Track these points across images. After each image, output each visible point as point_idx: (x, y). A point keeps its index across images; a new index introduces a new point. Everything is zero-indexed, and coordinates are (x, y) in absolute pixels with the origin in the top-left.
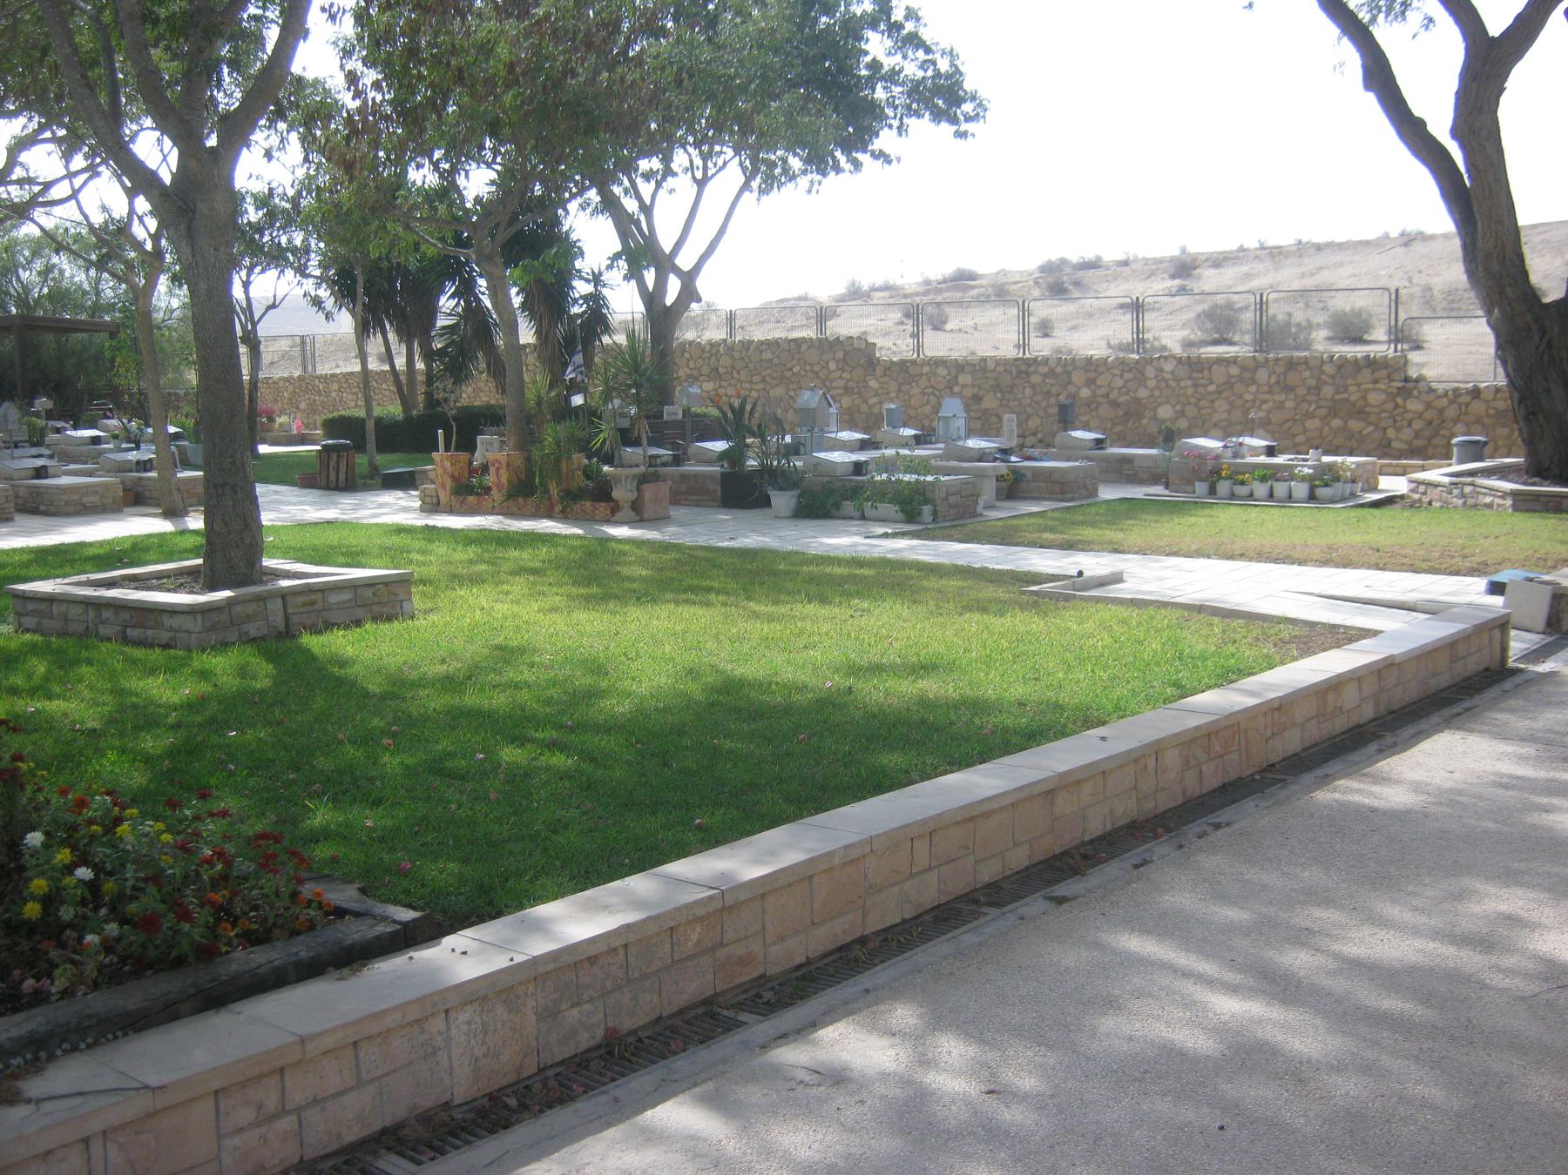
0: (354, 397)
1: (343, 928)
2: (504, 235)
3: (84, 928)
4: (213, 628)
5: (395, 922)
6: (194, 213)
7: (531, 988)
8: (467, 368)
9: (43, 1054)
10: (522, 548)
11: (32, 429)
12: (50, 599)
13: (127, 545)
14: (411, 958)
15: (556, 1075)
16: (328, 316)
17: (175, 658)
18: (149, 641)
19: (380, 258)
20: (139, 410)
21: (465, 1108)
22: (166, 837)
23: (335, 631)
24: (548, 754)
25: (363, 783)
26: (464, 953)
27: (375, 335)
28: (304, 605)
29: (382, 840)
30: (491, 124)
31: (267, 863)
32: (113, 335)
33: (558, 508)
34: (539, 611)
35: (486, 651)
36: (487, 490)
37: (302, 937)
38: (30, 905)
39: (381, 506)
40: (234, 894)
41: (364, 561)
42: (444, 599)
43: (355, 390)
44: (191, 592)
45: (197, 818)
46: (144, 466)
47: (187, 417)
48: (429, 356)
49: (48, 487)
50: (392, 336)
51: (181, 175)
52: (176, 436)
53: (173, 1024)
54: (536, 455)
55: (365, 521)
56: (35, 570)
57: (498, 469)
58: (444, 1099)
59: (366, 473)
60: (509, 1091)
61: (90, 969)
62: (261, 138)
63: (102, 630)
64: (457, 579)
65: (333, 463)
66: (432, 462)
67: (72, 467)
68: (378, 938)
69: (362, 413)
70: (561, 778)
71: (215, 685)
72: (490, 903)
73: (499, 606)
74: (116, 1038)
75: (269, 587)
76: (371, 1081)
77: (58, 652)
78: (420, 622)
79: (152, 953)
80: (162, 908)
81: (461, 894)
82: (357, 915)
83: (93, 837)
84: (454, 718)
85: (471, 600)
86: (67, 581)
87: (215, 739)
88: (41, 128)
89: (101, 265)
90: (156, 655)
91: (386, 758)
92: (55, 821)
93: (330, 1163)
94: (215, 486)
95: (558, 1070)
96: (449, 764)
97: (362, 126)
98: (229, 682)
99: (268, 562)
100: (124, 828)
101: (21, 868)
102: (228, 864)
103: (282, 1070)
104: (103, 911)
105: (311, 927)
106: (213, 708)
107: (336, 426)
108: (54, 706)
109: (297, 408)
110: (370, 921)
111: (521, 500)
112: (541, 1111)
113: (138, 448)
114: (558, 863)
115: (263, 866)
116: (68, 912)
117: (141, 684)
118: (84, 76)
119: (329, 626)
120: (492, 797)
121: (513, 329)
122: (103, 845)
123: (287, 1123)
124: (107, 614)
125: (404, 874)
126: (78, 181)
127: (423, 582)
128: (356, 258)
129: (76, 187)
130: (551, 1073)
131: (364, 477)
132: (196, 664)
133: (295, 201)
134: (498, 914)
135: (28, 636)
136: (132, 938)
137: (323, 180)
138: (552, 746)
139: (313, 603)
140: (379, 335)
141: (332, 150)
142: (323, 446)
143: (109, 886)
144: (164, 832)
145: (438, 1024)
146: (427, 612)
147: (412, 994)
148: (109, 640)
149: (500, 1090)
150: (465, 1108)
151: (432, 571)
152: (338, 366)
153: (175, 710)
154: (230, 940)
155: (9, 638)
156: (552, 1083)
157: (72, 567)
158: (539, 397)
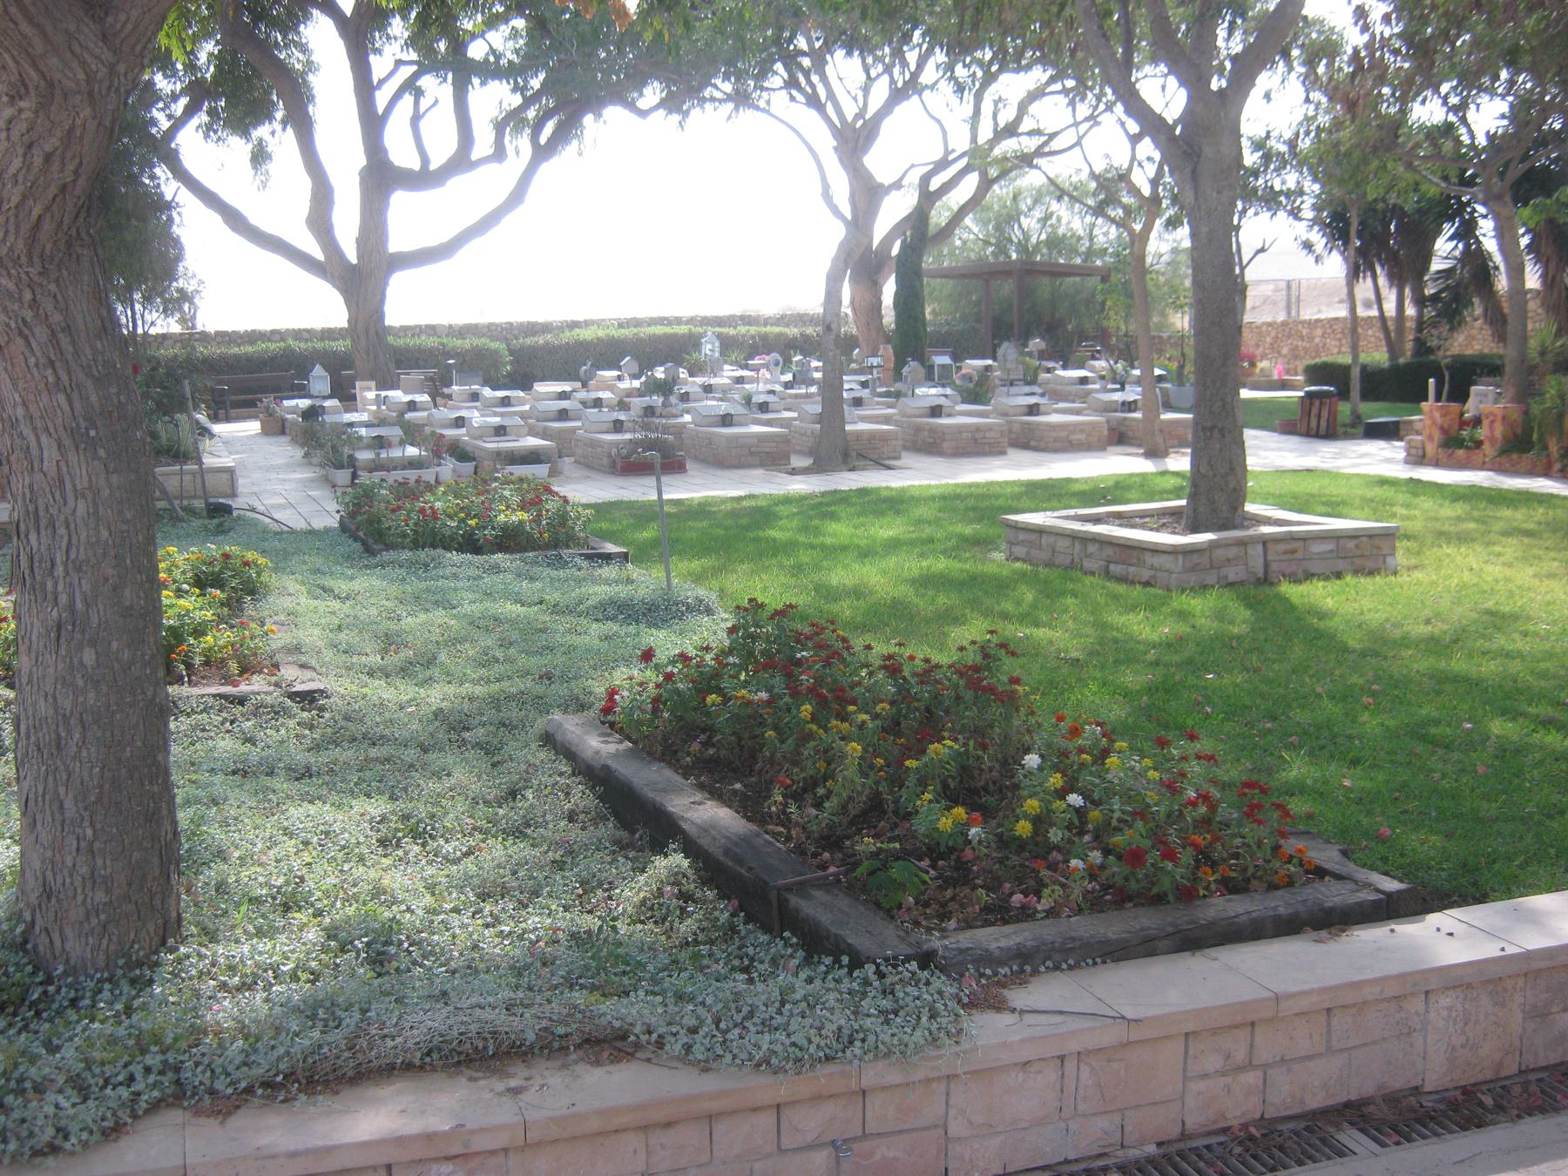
0: (1338, 343)
1: (1323, 889)
2: (1517, 170)
3: (1069, 852)
4: (1193, 569)
5: (1378, 890)
6: (1199, 157)
7: (1521, 982)
8: (1460, 314)
9: (1028, 968)
10: (1516, 508)
11: (1027, 368)
12: (1040, 531)
13: (1111, 483)
14: (1392, 931)
15: (1538, 1080)
16: (1318, 259)
17: (1155, 596)
18: (1130, 577)
19: (1376, 200)
20: (1128, 354)
21: (1435, 1097)
22: (1153, 774)
23: (1315, 581)
24: (1542, 732)
25: (1340, 740)
26: (1451, 934)
27: (1364, 278)
28: (1285, 553)
29: (1360, 801)
30: (1509, 52)
31: (1252, 812)
32: (1104, 279)
33: (1557, 466)
34: (1535, 576)
35: (1474, 615)
36: (1479, 444)
37: (1280, 892)
38: (1022, 823)
39: (1362, 456)
40: (1216, 839)
41: (1345, 511)
42: (1430, 555)
43: (1339, 336)
44: (1174, 533)
45: (1184, 758)
46: (1129, 406)
47: (1169, 359)
48: (1420, 301)
49: (1039, 424)
50: (1382, 281)
51: (1187, 117)
52: (1160, 378)
53: (1148, 959)
54: (1535, 409)
55: (1346, 471)
56: (1025, 503)
57: (1492, 422)
58: (1414, 1084)
59: (1348, 421)
60: (1484, 1088)
61: (1076, 893)
62: (1265, 80)
63: (1087, 564)
64: (1442, 536)
65: (1315, 411)
66: (1420, 412)
67: (1062, 405)
68: (1360, 904)
69: (1346, 359)
70: (1557, 760)
71: (1194, 627)
72: (1475, 884)
73: (1490, 568)
74: (1095, 963)
75: (1251, 532)
76: (1341, 1050)
77: (1046, 582)
78: (1404, 578)
79: (1133, 886)
80: (1146, 843)
81: (1443, 870)
82: (1339, 877)
83: (1083, 765)
84: (1440, 682)
85: (1459, 559)
86: (1056, 514)
87: (1192, 680)
88: (1052, 80)
89: (1099, 211)
90: (1137, 592)
91: (1365, 717)
92: (1049, 746)
93: (1291, 1125)
94: (1204, 429)
95: (1540, 1075)
96: (1433, 730)
97: (1368, 66)
98: (1207, 625)
99: (1250, 508)
100: (1113, 760)
101: (1016, 787)
102: (1213, 808)
103: (1253, 1024)
104: (1087, 838)
105: (1290, 883)
106: (1190, 650)
107: (1319, 373)
108: (1041, 633)
109: (1279, 352)
110: (1350, 886)
111: (1515, 456)
112: (1519, 1117)
113: (1122, 389)
114: (1552, 851)
115: (1248, 815)
116: (1056, 835)
117: (1123, 619)
118: (1101, 27)
119: (1309, 576)
120: (1480, 771)
121: (1517, 273)
122: (1091, 773)
123: (1252, 1078)
124: (1092, 548)
125: (1380, 839)
126: (1083, 128)
127: (1408, 537)
128: (1351, 200)
129: (1081, 134)
130: (1532, 1077)
131: (1345, 426)
132: (1175, 604)
133: (1292, 144)
134: (1481, 899)
135: (1018, 565)
136: (1115, 869)
137: (1324, 120)
138: (1546, 723)
139: (1293, 552)
140: (1369, 280)
141: (1336, 88)
142: (1307, 393)
143: (1095, 814)
144: (1150, 768)
145: (1417, 1004)
146: (1410, 569)
147: (1394, 969)
148: (1093, 573)
149: (1473, 1085)
150: (1435, 1097)
151: (1416, 526)
152: (1319, 311)
153: (1154, 647)
154: (1209, 883)
155: (1001, 566)
156: (1533, 1088)
157: (1059, 501)
158: (1542, 345)
